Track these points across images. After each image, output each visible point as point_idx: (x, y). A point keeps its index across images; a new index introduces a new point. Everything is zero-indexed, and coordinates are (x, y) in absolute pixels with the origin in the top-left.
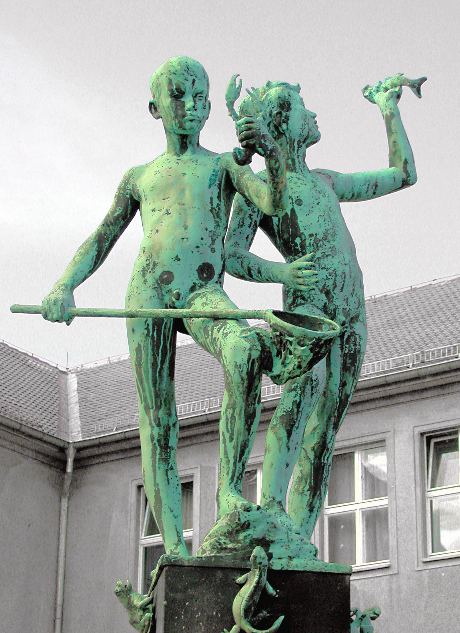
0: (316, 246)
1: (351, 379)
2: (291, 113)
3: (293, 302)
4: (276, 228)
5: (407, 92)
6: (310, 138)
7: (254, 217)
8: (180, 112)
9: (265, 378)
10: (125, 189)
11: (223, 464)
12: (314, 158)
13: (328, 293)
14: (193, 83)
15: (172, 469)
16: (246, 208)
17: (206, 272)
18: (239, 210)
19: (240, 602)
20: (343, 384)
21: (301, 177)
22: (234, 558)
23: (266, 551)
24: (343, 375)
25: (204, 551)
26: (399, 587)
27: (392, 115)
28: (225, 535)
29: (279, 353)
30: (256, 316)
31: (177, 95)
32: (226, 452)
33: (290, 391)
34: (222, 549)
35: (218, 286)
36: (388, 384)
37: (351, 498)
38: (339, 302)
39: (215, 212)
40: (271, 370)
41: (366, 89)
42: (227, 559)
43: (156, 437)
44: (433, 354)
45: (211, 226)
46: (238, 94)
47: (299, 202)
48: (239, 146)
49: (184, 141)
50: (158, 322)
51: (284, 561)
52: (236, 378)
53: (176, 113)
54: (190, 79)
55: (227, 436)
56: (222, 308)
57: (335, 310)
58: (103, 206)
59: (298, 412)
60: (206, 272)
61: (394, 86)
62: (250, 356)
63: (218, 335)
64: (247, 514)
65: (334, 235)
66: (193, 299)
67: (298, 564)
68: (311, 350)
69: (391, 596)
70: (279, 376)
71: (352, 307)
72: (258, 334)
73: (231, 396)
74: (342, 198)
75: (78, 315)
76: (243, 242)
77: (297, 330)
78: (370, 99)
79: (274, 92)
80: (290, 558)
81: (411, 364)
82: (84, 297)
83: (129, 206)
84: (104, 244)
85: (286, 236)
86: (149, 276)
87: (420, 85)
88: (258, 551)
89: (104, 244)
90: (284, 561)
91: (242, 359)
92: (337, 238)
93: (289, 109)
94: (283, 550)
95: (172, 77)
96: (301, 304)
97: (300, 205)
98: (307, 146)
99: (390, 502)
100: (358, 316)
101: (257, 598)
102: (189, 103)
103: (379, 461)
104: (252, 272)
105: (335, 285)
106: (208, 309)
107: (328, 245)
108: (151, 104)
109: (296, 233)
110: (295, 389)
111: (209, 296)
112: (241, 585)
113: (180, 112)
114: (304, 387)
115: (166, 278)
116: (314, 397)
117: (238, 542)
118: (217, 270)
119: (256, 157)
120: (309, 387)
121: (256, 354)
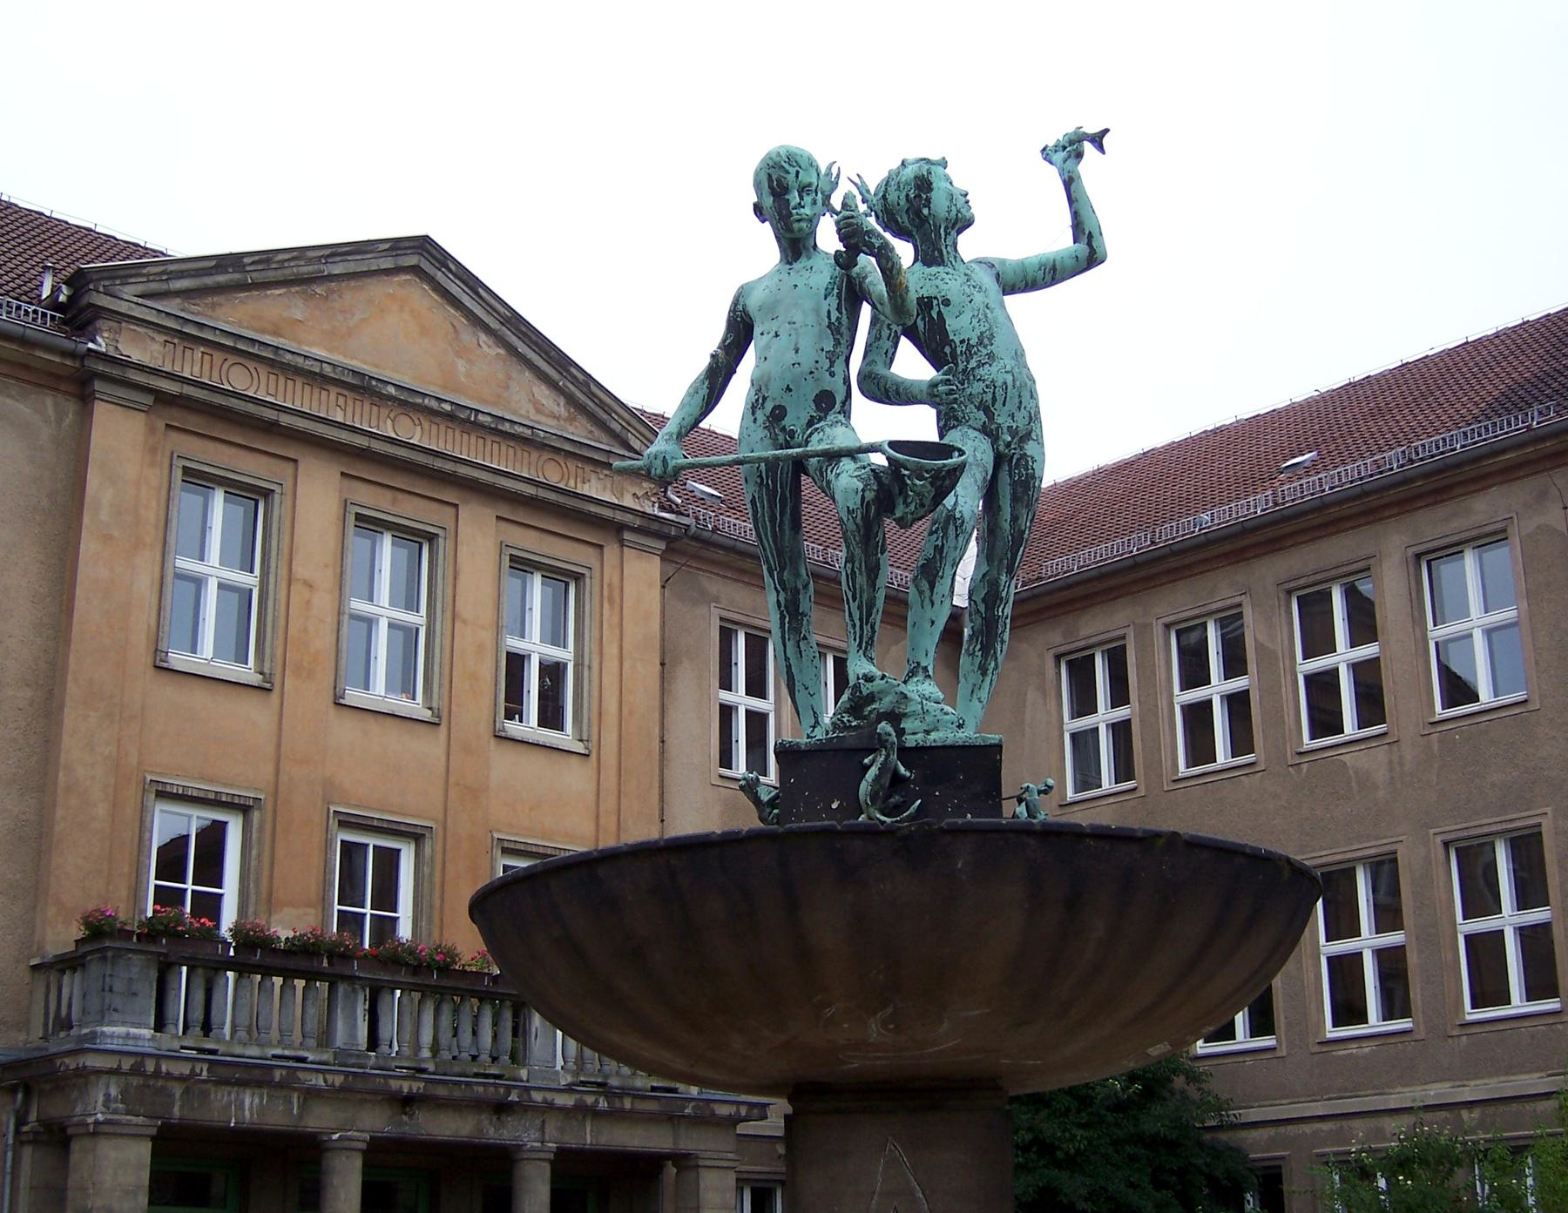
0: (969, 354)
2: (933, 195)
5: (1088, 147)
6: (962, 223)
11: (850, 628)
12: (969, 245)
15: (805, 638)
19: (864, 788)
20: (1015, 519)
26: (1401, 757)
32: (850, 615)
33: (931, 534)
35: (841, 417)
38: (1002, 419)
45: (829, 346)
47: (947, 302)
49: (795, 245)
50: (772, 464)
52: (851, 526)
54: (793, 171)
58: (714, 333)
61: (1071, 143)
62: (863, 497)
63: (831, 476)
64: (869, 685)
65: (992, 337)
67: (936, 737)
69: (1391, 770)
71: (1021, 422)
74: (1010, 289)
76: (880, 360)
78: (1048, 159)
79: (910, 172)
80: (927, 732)
83: (740, 330)
88: (885, 727)
90: (920, 736)
91: (854, 502)
92: (997, 341)
93: (930, 189)
98: (959, 232)
100: (1029, 434)
101: (886, 781)
102: (794, 198)
104: (888, 392)
105: (994, 399)
107: (984, 352)
111: (827, 430)
112: (868, 768)
115: (778, 414)
117: (865, 718)
120: (951, 527)
121: (870, 495)
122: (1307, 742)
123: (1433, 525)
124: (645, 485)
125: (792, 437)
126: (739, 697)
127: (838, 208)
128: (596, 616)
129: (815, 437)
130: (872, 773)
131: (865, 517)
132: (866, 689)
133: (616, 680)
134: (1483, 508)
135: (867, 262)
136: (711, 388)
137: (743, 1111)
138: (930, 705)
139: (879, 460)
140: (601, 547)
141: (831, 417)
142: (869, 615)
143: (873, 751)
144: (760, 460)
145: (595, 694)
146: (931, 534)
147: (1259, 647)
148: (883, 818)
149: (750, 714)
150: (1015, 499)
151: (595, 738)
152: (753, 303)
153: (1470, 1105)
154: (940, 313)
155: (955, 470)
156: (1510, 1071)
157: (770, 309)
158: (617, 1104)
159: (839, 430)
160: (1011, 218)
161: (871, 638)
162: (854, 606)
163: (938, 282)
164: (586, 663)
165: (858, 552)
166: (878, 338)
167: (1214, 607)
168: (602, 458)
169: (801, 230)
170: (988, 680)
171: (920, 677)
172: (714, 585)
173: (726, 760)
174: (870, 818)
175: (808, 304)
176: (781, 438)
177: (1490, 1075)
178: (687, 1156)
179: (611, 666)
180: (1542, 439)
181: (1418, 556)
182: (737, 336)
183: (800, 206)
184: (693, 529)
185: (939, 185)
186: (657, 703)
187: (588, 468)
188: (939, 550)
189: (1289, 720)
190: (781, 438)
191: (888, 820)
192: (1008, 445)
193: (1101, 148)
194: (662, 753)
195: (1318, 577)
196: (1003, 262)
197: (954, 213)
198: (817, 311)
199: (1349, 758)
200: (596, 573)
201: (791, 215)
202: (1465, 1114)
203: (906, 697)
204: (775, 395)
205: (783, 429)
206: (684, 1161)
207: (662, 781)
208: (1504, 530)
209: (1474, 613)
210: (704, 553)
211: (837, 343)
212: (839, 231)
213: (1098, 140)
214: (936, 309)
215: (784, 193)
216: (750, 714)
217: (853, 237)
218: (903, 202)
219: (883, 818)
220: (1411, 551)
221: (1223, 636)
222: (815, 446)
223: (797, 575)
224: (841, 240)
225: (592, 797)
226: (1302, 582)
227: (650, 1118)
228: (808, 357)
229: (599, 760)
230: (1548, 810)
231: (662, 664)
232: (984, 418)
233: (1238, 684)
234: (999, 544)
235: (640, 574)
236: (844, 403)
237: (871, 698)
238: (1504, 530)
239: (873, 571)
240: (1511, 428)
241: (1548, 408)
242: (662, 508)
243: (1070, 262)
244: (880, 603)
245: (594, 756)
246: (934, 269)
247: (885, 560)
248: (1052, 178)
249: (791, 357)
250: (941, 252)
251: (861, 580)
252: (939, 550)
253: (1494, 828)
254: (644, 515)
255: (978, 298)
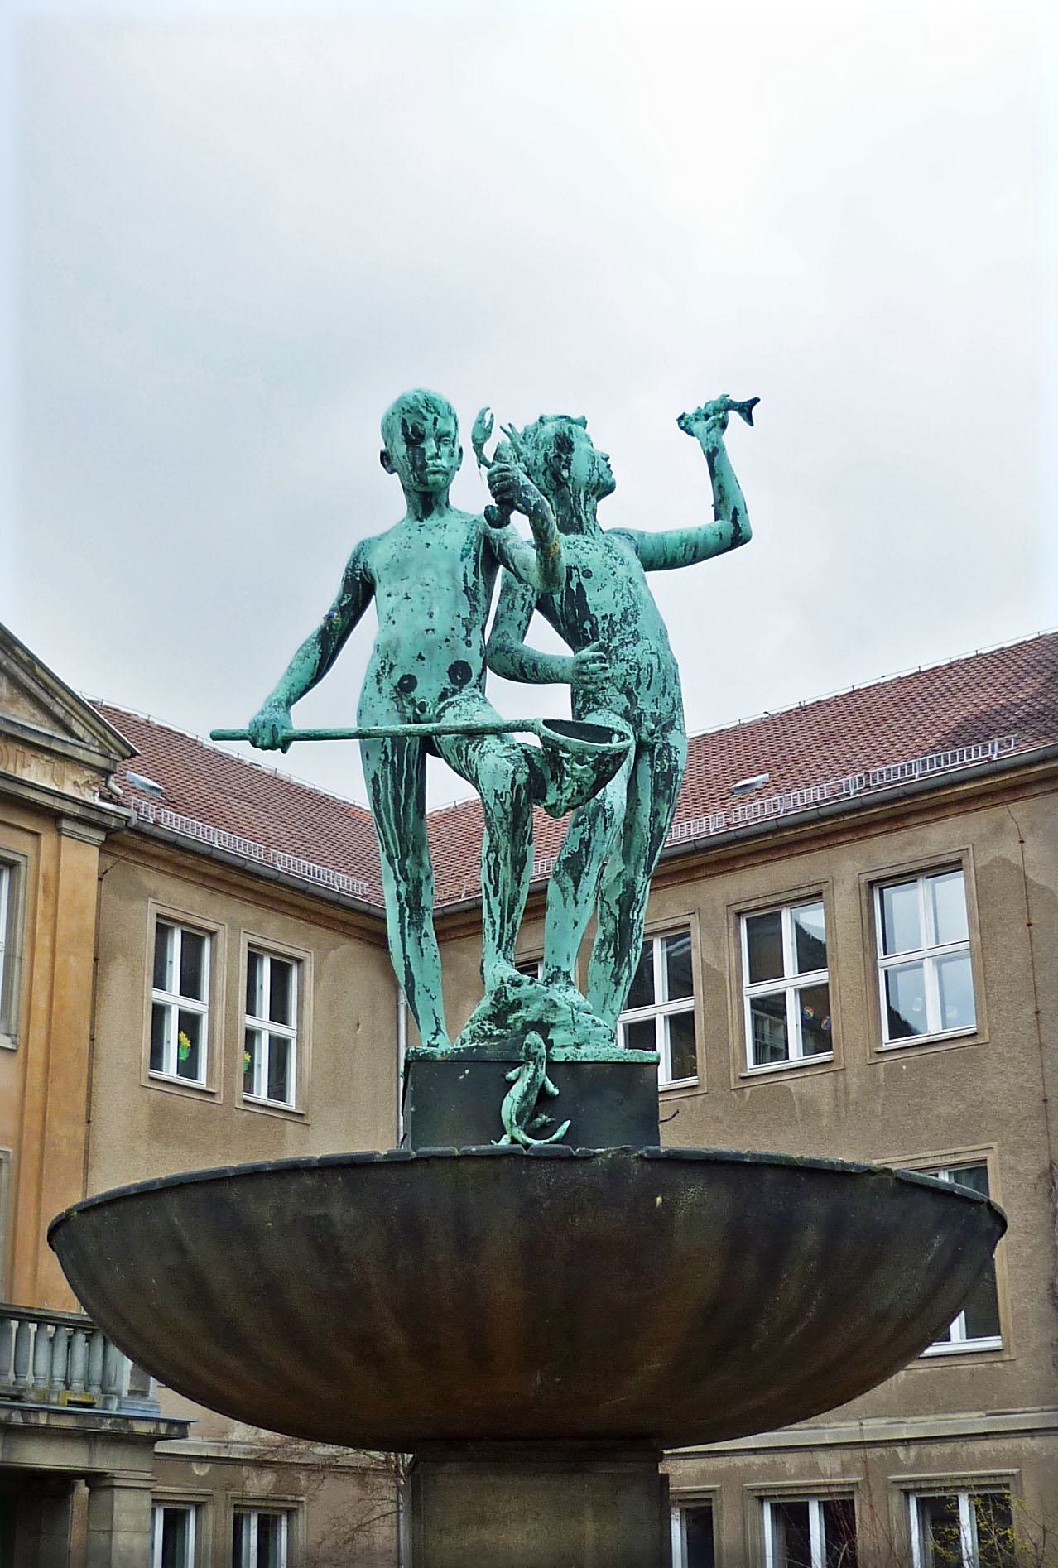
0: (612, 632)
1: (666, 806)
2: (574, 456)
3: (584, 708)
4: (558, 610)
5: (734, 416)
6: (604, 489)
7: (528, 597)
8: (419, 463)
9: (538, 810)
10: (353, 569)
12: (608, 513)
13: (629, 693)
14: (435, 423)
16: (517, 585)
17: (459, 673)
18: (507, 589)
19: (509, 1106)
20: (656, 814)
21: (590, 539)
22: (503, 1048)
23: (544, 1037)
24: (653, 802)
25: (463, 1041)
27: (716, 450)
28: (489, 1018)
29: (554, 776)
30: (523, 727)
31: (414, 439)
33: (576, 825)
34: (486, 1037)
35: (477, 691)
36: (823, 818)
37: (780, 974)
38: (646, 706)
39: (470, 593)
40: (544, 800)
41: (682, 418)
42: (492, 1049)
43: (403, 895)
44: (882, 776)
45: (465, 613)
46: (487, 433)
47: (588, 574)
48: (492, 502)
49: (427, 499)
50: (398, 739)
51: (569, 1050)
52: (498, 812)
53: (413, 464)
54: (431, 417)
55: (491, 888)
56: (481, 719)
57: (640, 715)
58: (328, 592)
59: (587, 852)
60: (459, 673)
61: (716, 411)
62: (514, 780)
63: (473, 755)
64: (516, 990)
66: (443, 710)
67: (587, 1053)
68: (593, 768)
70: (555, 806)
71: (664, 709)
72: (524, 751)
73: (492, 836)
74: (650, 565)
75: (296, 739)
76: (513, 632)
77: (575, 743)
79: (549, 430)
80: (578, 1046)
81: (852, 791)
82: (302, 717)
83: (359, 589)
84: (330, 642)
85: (571, 620)
86: (385, 683)
87: (751, 408)
88: (534, 1038)
89: (330, 642)
90: (569, 1050)
93: (571, 449)
94: (566, 1035)
95: (406, 416)
96: (594, 710)
97: (588, 577)
98: (598, 499)
99: (831, 974)
101: (533, 1098)
102: (430, 446)
103: (814, 919)
104: (527, 671)
105: (638, 682)
106: (461, 723)
107: (629, 629)
108: (383, 454)
109: (585, 614)
110: (582, 823)
112: (513, 1082)
113: (419, 463)
114: (595, 820)
115: (407, 684)
116: (609, 832)
117: (508, 1026)
118: (476, 670)
119: (515, 516)
120: (600, 819)
121: (521, 779)
122: (751, 1068)
123: (888, 850)
124: (87, 773)
125: (423, 711)
126: (172, 997)
127: (490, 460)
128: (30, 907)
129: (450, 712)
130: (518, 1090)
131: (515, 804)
132: (512, 994)
133: (47, 974)
134: (936, 838)
135: (520, 526)
136: (323, 653)
137: (163, 1429)
138: (580, 1016)
139: (532, 741)
140: (37, 834)
141: (467, 691)
142: (511, 911)
143: (520, 1064)
144: (387, 734)
145: (26, 986)
146: (576, 825)
147: (705, 967)
148: (529, 1140)
149: (183, 1015)
150: (657, 793)
151: (22, 1033)
152: (376, 563)
153: (906, 1442)
154: (579, 585)
155: (619, 755)
156: (950, 1408)
157: (399, 568)
158: (32, 1420)
159: (475, 705)
160: (652, 489)
161: (512, 938)
162: (494, 901)
163: (578, 551)
164: (18, 954)
165: (504, 841)
166: (511, 609)
167: (661, 926)
168: (44, 743)
169: (436, 483)
170: (621, 989)
171: (562, 983)
172: (150, 880)
173: (156, 1059)
174: (514, 1141)
175: (444, 566)
176: (409, 712)
177: (927, 1413)
178: (101, 1476)
179: (42, 957)
180: (1002, 771)
181: (871, 884)
182: (355, 597)
183: (437, 456)
184: (134, 821)
185: (579, 445)
186: (88, 1000)
187: (28, 753)
188: (586, 843)
189: (734, 1041)
190: (409, 712)
191: (536, 1142)
192: (651, 733)
193: (749, 419)
194: (92, 1050)
195: (769, 900)
196: (642, 535)
197: (596, 477)
198: (452, 573)
199: (793, 1084)
200: (32, 862)
201: (425, 465)
202: (901, 1451)
203: (555, 1005)
204: (404, 664)
205: (412, 701)
206: (97, 1480)
207: (90, 1079)
208: (960, 862)
209: (932, 939)
210: (146, 847)
211: (474, 610)
212: (490, 486)
213: (746, 410)
214: (575, 580)
215: (416, 446)
216: (183, 1015)
217: (506, 497)
218: (540, 462)
219: (529, 1140)
220: (864, 879)
221: (669, 954)
222: (450, 720)
223: (421, 865)
224: (494, 495)
225: (16, 1095)
226: (752, 904)
227: (65, 1435)
228: (442, 622)
229: (26, 1056)
230: (994, 1145)
231: (96, 959)
232: (626, 702)
233: (683, 1005)
234: (637, 841)
235: (79, 860)
236: (480, 677)
237: (517, 1005)
238: (960, 862)
239: (519, 863)
240: (972, 758)
241: (1009, 742)
242: (102, 798)
243: (713, 540)
244: (523, 899)
245: (21, 1051)
246: (572, 537)
247: (531, 850)
248: (692, 451)
249: (423, 622)
250: (579, 519)
251: (505, 873)
252: (586, 843)
253: (938, 1161)
254: (85, 805)
255: (621, 571)
